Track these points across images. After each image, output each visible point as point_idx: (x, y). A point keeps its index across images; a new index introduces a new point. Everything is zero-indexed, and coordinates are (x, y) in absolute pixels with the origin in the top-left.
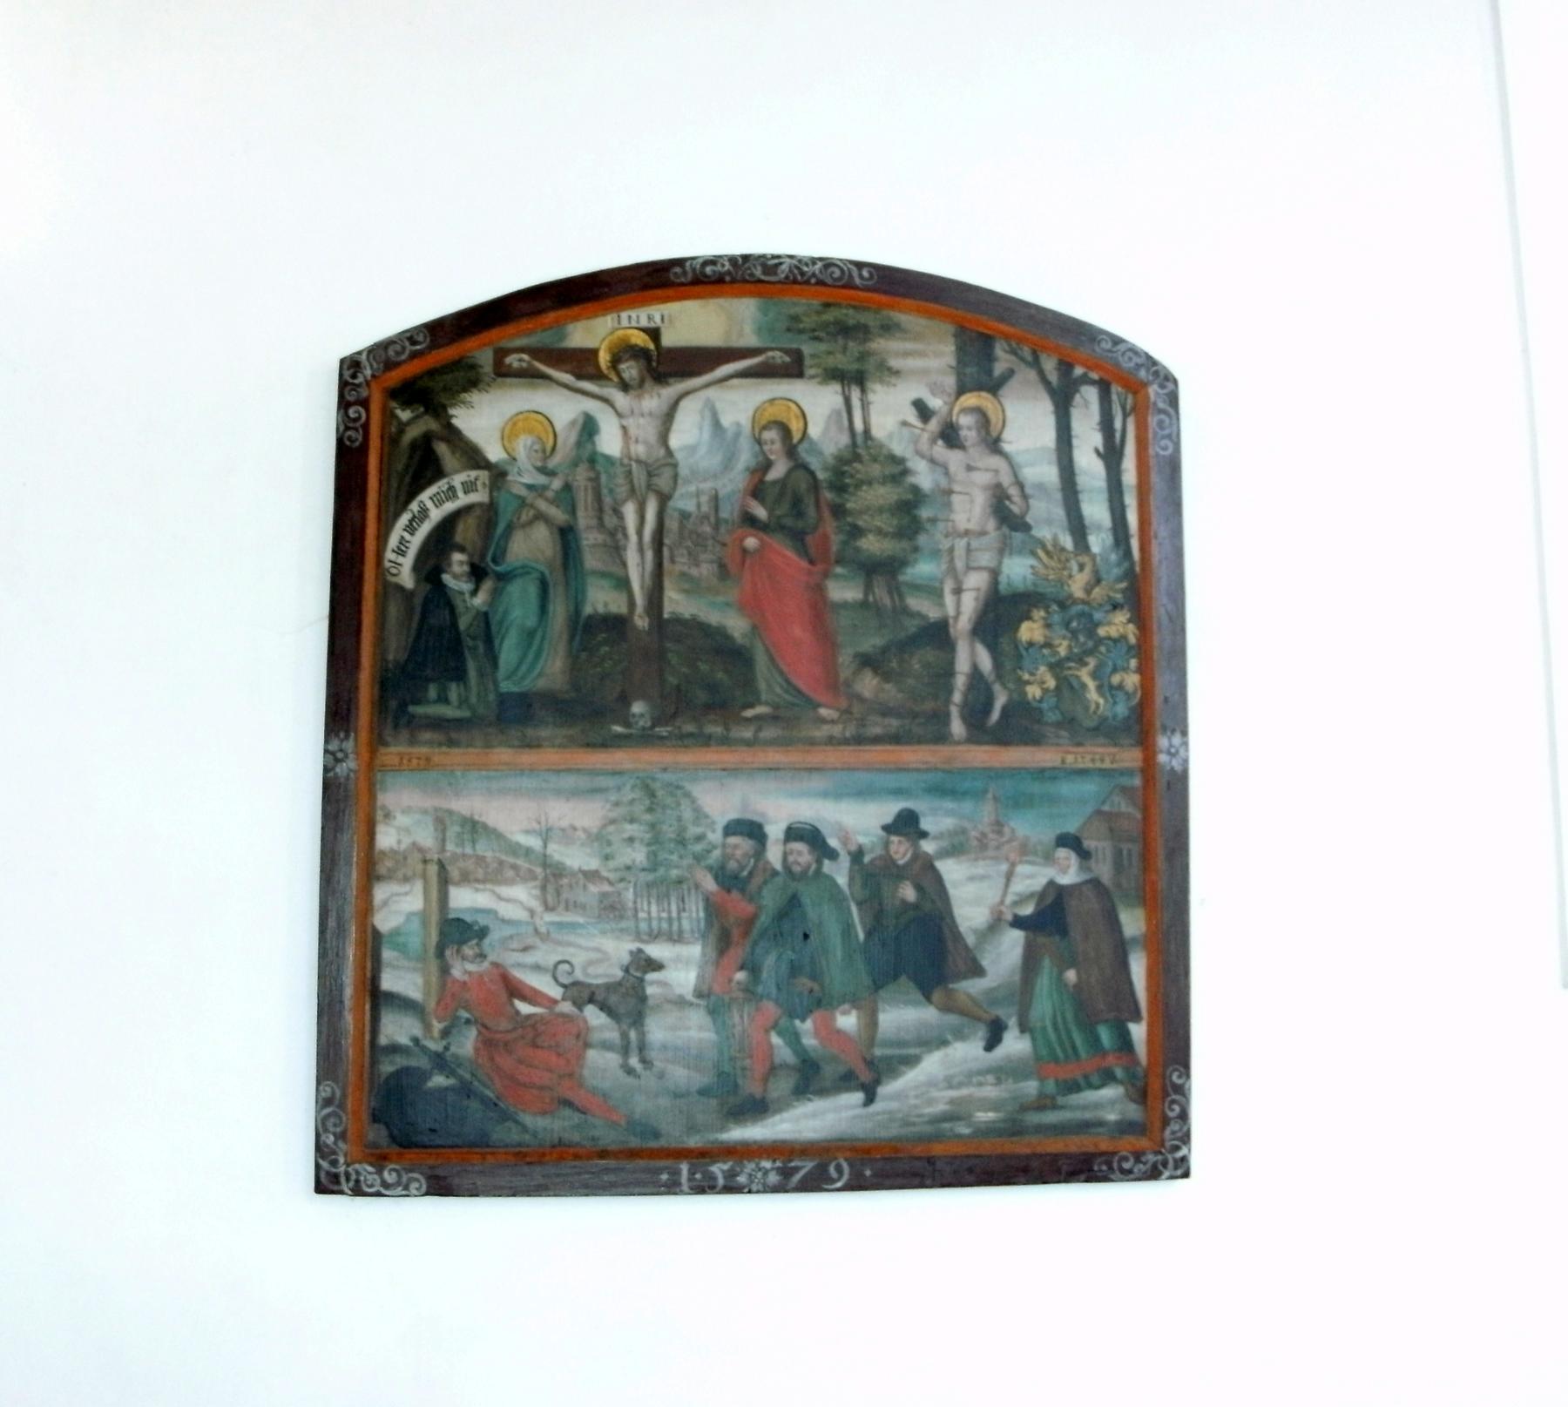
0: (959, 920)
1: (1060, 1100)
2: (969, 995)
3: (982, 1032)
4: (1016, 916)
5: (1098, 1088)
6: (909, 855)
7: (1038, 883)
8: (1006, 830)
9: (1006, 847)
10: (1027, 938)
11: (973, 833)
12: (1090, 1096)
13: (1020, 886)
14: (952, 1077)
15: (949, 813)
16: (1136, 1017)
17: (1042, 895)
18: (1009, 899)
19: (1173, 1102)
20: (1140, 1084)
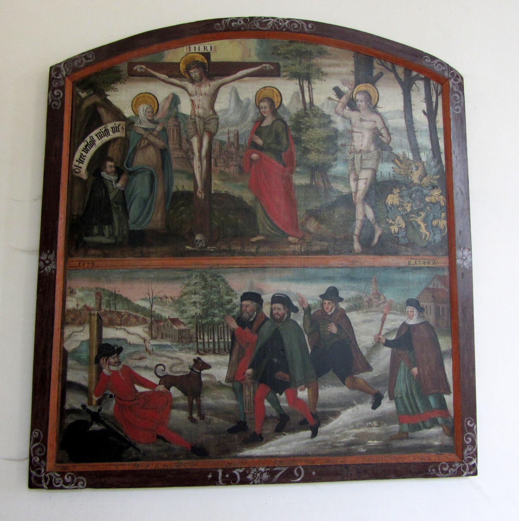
1: (410, 434)
2: (364, 381)
3: (371, 399)
5: (429, 428)
7: (397, 324)
8: (382, 297)
11: (365, 299)
12: (426, 432)
13: (388, 326)
14: (357, 422)
16: (448, 392)
18: (384, 332)
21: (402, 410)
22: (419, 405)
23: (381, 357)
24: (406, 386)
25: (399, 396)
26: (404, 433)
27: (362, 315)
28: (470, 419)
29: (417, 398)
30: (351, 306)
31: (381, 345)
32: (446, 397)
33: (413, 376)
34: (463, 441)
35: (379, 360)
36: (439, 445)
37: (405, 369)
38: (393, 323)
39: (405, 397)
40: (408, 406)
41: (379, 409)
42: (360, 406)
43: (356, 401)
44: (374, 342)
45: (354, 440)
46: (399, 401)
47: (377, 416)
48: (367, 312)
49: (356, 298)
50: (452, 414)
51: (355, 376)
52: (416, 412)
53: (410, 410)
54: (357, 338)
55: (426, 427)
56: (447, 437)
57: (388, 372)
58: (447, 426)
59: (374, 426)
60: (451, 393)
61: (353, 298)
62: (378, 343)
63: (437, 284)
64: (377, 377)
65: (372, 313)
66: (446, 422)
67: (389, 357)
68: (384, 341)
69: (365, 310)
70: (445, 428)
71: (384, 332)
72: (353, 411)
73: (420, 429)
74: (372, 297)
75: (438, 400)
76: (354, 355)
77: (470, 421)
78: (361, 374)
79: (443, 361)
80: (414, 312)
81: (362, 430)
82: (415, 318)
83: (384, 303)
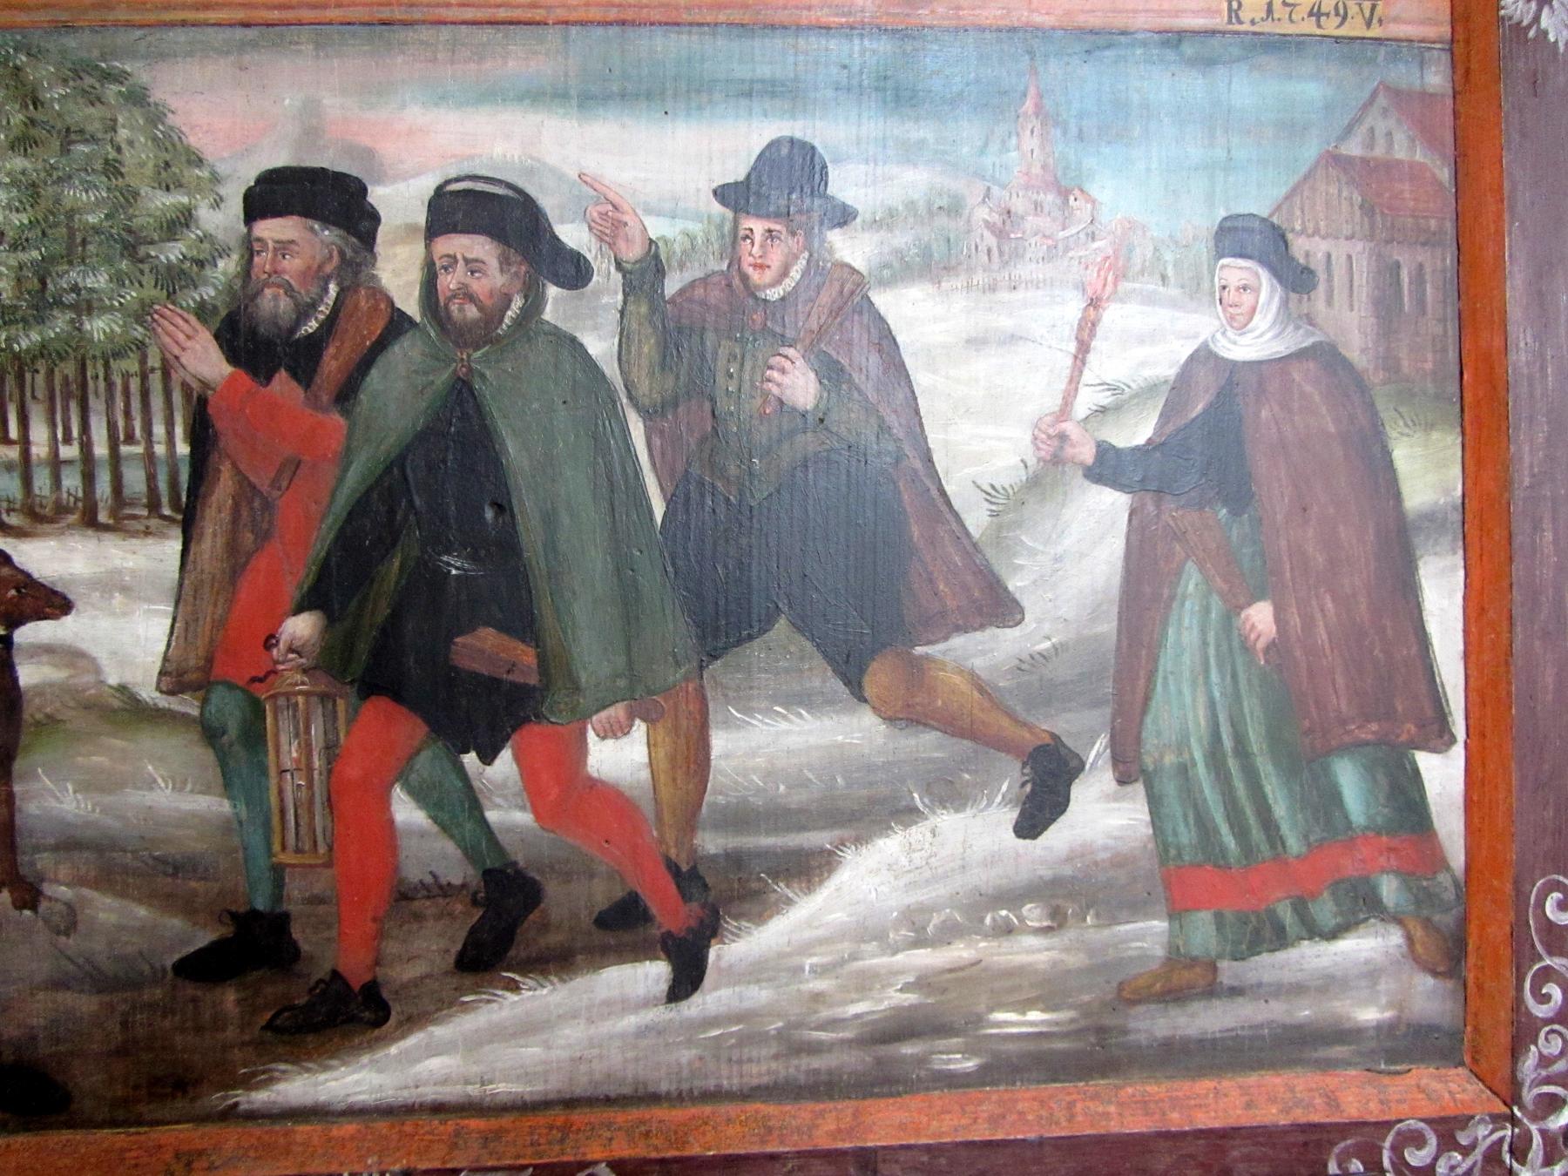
1: (1229, 971)
5: (1333, 935)
7: (1165, 361)
11: (982, 213)
14: (926, 909)
16: (1439, 738)
18: (1085, 402)
19: (1547, 974)
21: (1186, 836)
22: (1280, 810)
24: (1212, 705)
26: (1193, 962)
28: (1558, 886)
29: (1266, 768)
30: (899, 253)
32: (1426, 761)
33: (1247, 648)
34: (1519, 1000)
36: (1379, 1027)
39: (1201, 769)
42: (948, 822)
43: (928, 789)
44: (1032, 462)
46: (1170, 788)
47: (1047, 873)
50: (1456, 855)
51: (919, 650)
52: (1265, 847)
53: (1230, 841)
55: (1316, 932)
57: (1108, 627)
58: (1427, 923)
61: (911, 205)
66: (1424, 899)
68: (1087, 454)
70: (1419, 933)
72: (910, 849)
73: (1281, 939)
75: (1382, 779)
78: (958, 642)
81: (960, 952)
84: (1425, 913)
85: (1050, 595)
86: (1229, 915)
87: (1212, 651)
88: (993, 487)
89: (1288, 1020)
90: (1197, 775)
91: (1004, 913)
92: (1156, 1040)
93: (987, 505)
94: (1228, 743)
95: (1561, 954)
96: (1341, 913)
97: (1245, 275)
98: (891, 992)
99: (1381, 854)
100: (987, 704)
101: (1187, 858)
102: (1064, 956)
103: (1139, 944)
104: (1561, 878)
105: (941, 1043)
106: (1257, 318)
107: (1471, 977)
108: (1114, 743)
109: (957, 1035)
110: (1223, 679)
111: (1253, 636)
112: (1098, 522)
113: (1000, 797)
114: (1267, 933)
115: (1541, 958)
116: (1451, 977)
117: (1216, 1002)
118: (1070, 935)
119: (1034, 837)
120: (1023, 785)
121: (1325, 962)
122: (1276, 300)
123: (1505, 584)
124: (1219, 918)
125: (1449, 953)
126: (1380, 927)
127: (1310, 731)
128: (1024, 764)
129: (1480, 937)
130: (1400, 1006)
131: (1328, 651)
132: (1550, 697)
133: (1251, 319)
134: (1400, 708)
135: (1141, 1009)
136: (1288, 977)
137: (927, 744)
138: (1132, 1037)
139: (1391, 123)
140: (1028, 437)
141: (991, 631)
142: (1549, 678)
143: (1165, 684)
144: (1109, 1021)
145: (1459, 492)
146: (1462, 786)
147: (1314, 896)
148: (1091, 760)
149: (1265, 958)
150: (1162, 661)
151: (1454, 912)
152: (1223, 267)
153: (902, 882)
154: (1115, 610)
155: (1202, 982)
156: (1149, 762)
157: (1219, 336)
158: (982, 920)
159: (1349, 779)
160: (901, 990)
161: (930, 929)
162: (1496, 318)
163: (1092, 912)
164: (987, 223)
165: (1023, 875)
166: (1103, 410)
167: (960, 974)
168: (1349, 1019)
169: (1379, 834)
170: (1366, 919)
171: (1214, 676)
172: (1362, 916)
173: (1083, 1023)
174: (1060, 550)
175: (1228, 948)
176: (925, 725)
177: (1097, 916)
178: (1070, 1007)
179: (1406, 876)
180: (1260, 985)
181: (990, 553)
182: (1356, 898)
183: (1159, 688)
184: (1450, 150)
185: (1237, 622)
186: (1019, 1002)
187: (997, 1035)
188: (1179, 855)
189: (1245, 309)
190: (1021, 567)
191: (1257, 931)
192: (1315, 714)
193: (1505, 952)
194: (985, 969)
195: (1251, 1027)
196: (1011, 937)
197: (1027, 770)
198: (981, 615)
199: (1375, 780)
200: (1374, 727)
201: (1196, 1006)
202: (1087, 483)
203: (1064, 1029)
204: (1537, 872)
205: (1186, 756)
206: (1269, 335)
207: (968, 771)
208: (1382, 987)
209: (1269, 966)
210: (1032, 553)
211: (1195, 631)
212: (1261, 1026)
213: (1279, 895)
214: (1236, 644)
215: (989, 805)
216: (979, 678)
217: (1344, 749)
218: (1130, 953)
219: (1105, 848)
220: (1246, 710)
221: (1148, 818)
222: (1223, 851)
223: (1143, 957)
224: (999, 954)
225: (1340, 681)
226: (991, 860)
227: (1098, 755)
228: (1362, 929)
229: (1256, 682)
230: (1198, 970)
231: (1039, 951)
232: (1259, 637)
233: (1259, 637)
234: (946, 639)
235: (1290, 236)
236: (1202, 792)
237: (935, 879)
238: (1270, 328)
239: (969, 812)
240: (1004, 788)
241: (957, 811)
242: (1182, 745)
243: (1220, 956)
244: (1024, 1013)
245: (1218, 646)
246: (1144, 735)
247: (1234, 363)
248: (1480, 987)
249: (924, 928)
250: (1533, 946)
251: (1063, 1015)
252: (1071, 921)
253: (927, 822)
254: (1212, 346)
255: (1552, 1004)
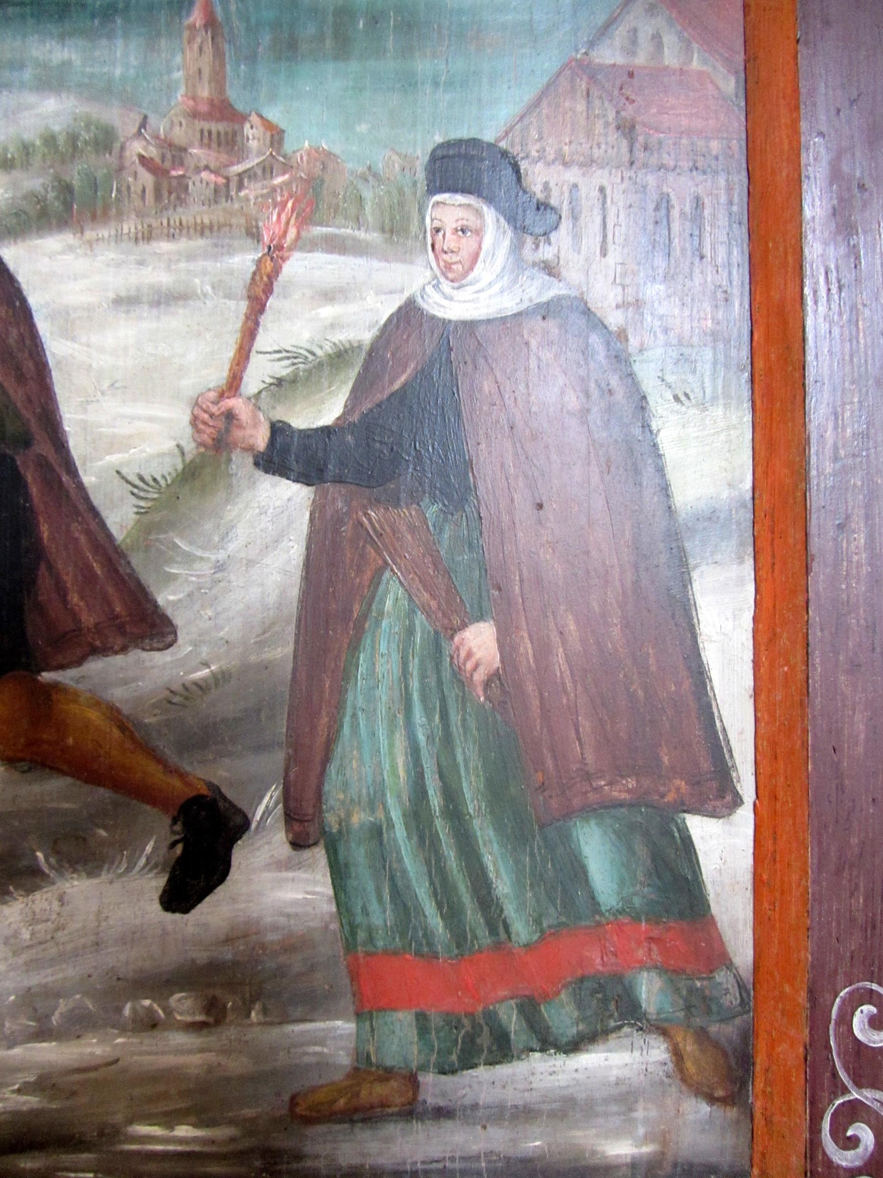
0: (77, 446)
1: (433, 1087)
2: (113, 713)
3: (156, 841)
4: (278, 429)
5: (574, 1046)
6: (438, 198)
7: (361, 320)
8: (253, 134)
9: (252, 191)
10: (317, 512)
11: (137, 147)
12: (546, 1073)
13: (295, 328)
14: (52, 994)
15: (52, 81)
16: (719, 797)
17: (377, 357)
18: (259, 373)
19: (854, 1111)
20: (726, 1031)
21: (379, 916)
22: (503, 886)
23: (232, 547)
24: (414, 751)
25: (359, 818)
26: (387, 1074)
27: (110, 254)
28: (870, 997)
29: (484, 831)
30: (32, 196)
31: (241, 464)
32: (700, 828)
33: (461, 679)
34: (814, 1143)
35: (220, 567)
36: (634, 1165)
37: (410, 631)
38: (327, 312)
39: (400, 831)
40: (422, 891)
41: (215, 912)
42: (79, 889)
43: (55, 848)
44: (190, 447)
45: (35, 1113)
46: (358, 854)
47: (202, 957)
48: (148, 236)
49: (73, 138)
50: (741, 947)
51: (47, 676)
52: (483, 933)
53: (436, 923)
54: (72, 417)
55: (547, 1042)
56: (698, 1110)
57: (282, 652)
58: (702, 1035)
59: (169, 1024)
60: (737, 801)
61: (50, 140)
62: (213, 452)
63: (657, 38)
64: (202, 687)
65: (183, 244)
66: (697, 1003)
67: (294, 551)
68: (261, 439)
69: (129, 226)
70: (689, 1047)
71: (259, 373)
72: (33, 920)
73: (502, 1050)
74: (179, 135)
75: (642, 850)
76: (45, 531)
77: (869, 1009)
78: (95, 666)
79: (685, 582)
80: (478, 232)
81: (92, 1048)
82: (484, 272)
83: (267, 170)
84: (697, 1021)
85: (210, 613)
86: (435, 1019)
87: (415, 684)
88: (142, 479)
89: (511, 1152)
90: (395, 840)
91: (147, 1002)
92: (340, 1168)
93: (134, 501)
94: (435, 801)
95: (874, 1086)
96: (584, 1019)
97: (461, 213)
98: (7, 1093)
99: (639, 944)
100: (128, 745)
101: (380, 943)
102: (223, 1060)
103: (317, 1049)
104: (875, 987)
105: (67, 1158)
106: (479, 265)
107: (758, 1106)
108: (286, 796)
109: (89, 1151)
110: (430, 719)
111: (469, 666)
112: (273, 518)
113: (143, 860)
114: (485, 1040)
115: (845, 1091)
116: (734, 1104)
117: (417, 1126)
118: (230, 1033)
119: (186, 910)
120: (173, 845)
121: (562, 1080)
122: (506, 243)
123: (801, 599)
124: (422, 1020)
125: (729, 1075)
126: (638, 1038)
127: (543, 787)
128: (175, 821)
129: (769, 1056)
130: (663, 1139)
131: (569, 685)
132: (861, 749)
133: (471, 268)
134: (666, 759)
135: (321, 1128)
136: (512, 1097)
137: (54, 791)
138: (309, 1163)
139: (659, 22)
140: (186, 418)
141: (136, 655)
142: (859, 725)
143: (355, 727)
144: (280, 1141)
145: (748, 484)
146: (750, 861)
147: (547, 997)
148: (258, 817)
149: (482, 1073)
150: (350, 697)
151: (738, 1021)
152: (438, 203)
153: (21, 960)
154: (292, 629)
155: (398, 1100)
156: (331, 820)
157: (429, 289)
158: (119, 1010)
159: (597, 852)
160: (19, 1091)
161: (55, 1019)
162: (790, 259)
163: (258, 1006)
164: (142, 158)
165: (172, 959)
166: (279, 382)
167: (92, 1075)
168: (594, 1153)
169: (637, 919)
170: (619, 1028)
171: (419, 716)
172: (612, 1024)
173: (246, 1144)
174: (221, 555)
175: (434, 1058)
176: (51, 768)
177: (265, 1011)
178: (231, 1122)
179: (671, 972)
180: (475, 1106)
181: (137, 561)
182: (605, 1001)
183: (346, 730)
184: (740, 58)
185: (447, 649)
186: (167, 1114)
187: (138, 1153)
188: (371, 939)
189: (464, 255)
190: (174, 577)
191: (471, 1039)
192: (550, 763)
193: (798, 1080)
194: (125, 1071)
195: (463, 1158)
196: (156, 1033)
197: (178, 827)
198: (124, 634)
199: (631, 850)
200: (631, 783)
201: (392, 1129)
202: (259, 474)
203: (224, 1149)
204: (840, 978)
205: (380, 815)
206: (497, 287)
207: (105, 828)
208: (639, 1114)
209: (486, 1082)
210: (189, 559)
211: (396, 657)
212: (477, 1158)
213: (503, 993)
214: (447, 674)
215: (128, 870)
216: (118, 711)
217: (589, 811)
218: (306, 1059)
219: (275, 928)
220: (460, 758)
221: (330, 891)
222: (428, 934)
223: (323, 1065)
224: (141, 1054)
225: (586, 725)
226: (131, 937)
227: (267, 812)
228: (613, 1038)
229: (472, 724)
230: (394, 1084)
231: (190, 1052)
232: (476, 667)
233: (476, 667)
234: (79, 662)
235: (523, 165)
236: (400, 860)
237: (62, 958)
238: (500, 276)
239: (105, 876)
240: (149, 848)
241: (91, 874)
242: (376, 800)
243: (424, 1068)
244: (172, 1128)
245: (423, 677)
246: (326, 788)
247: (446, 323)
248: (768, 1121)
249: (48, 1017)
250: (835, 1075)
251: (222, 1133)
252: (230, 1017)
253: (54, 887)
254: (419, 300)
255: (860, 1150)
